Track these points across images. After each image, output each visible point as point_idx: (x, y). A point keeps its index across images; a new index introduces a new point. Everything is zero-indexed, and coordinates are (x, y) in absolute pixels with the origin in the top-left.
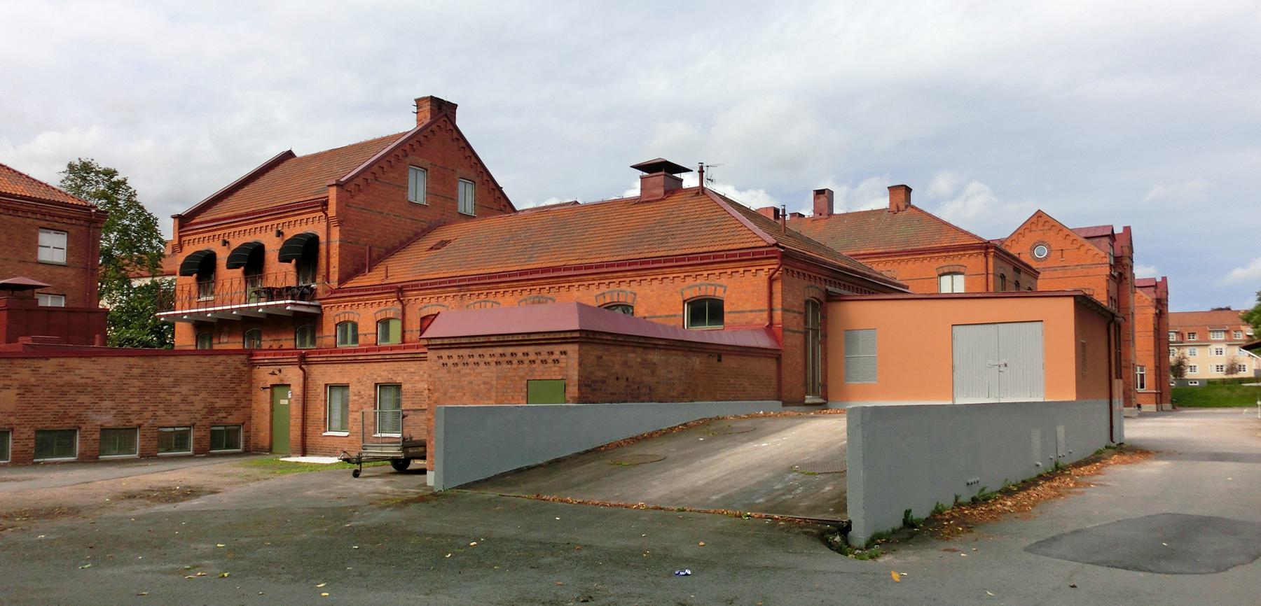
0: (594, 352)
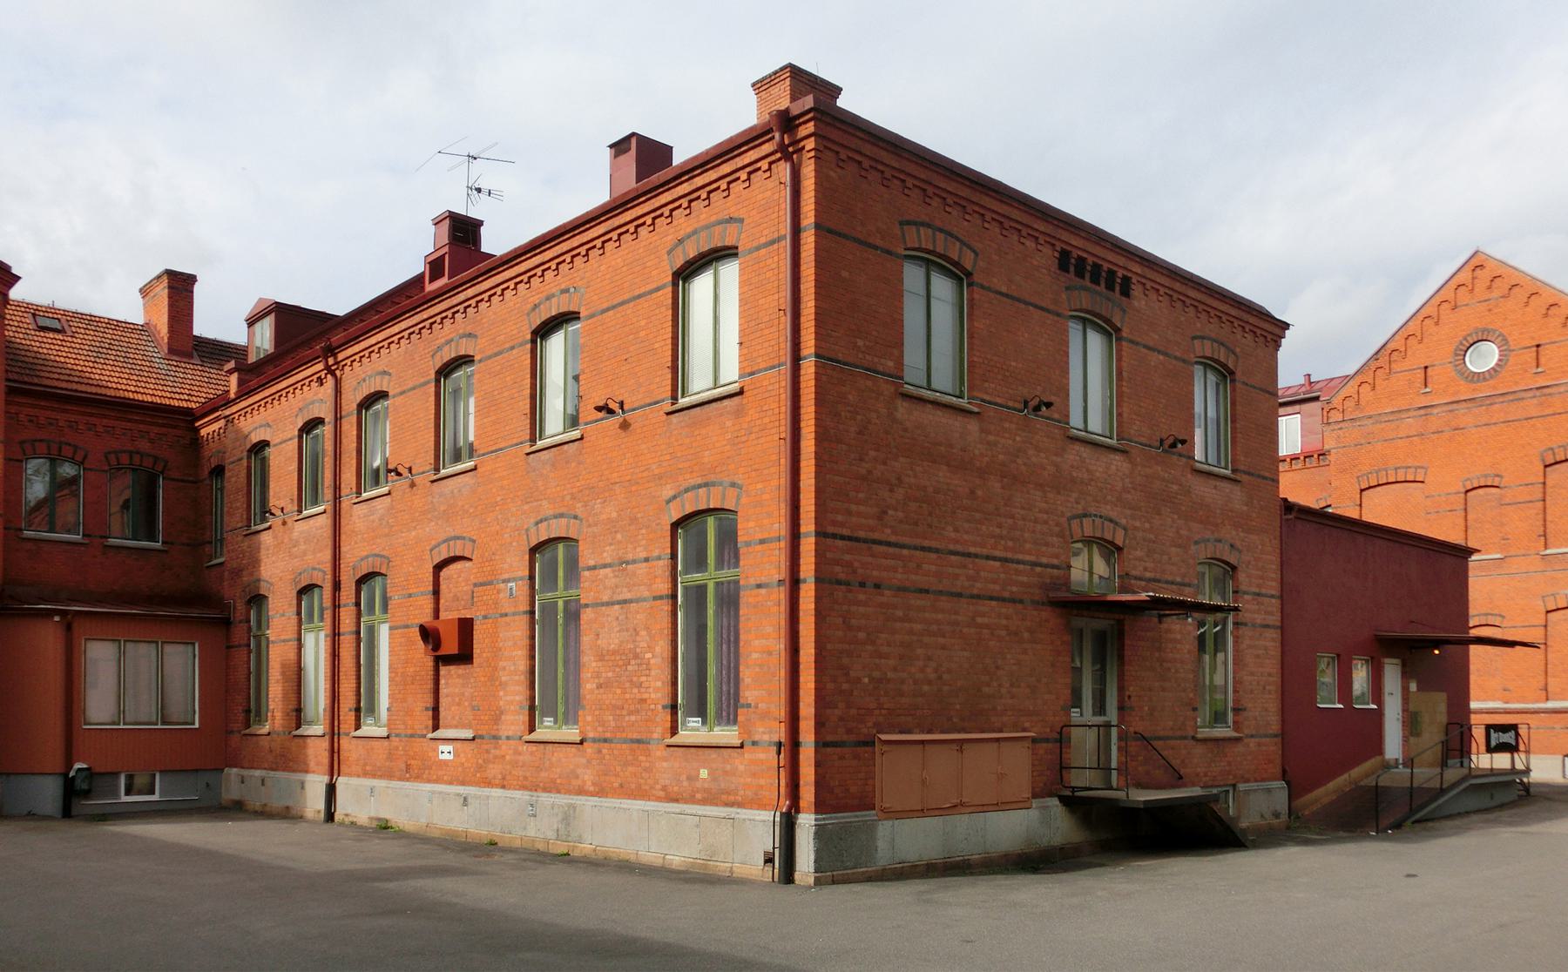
0: (1415, 765)
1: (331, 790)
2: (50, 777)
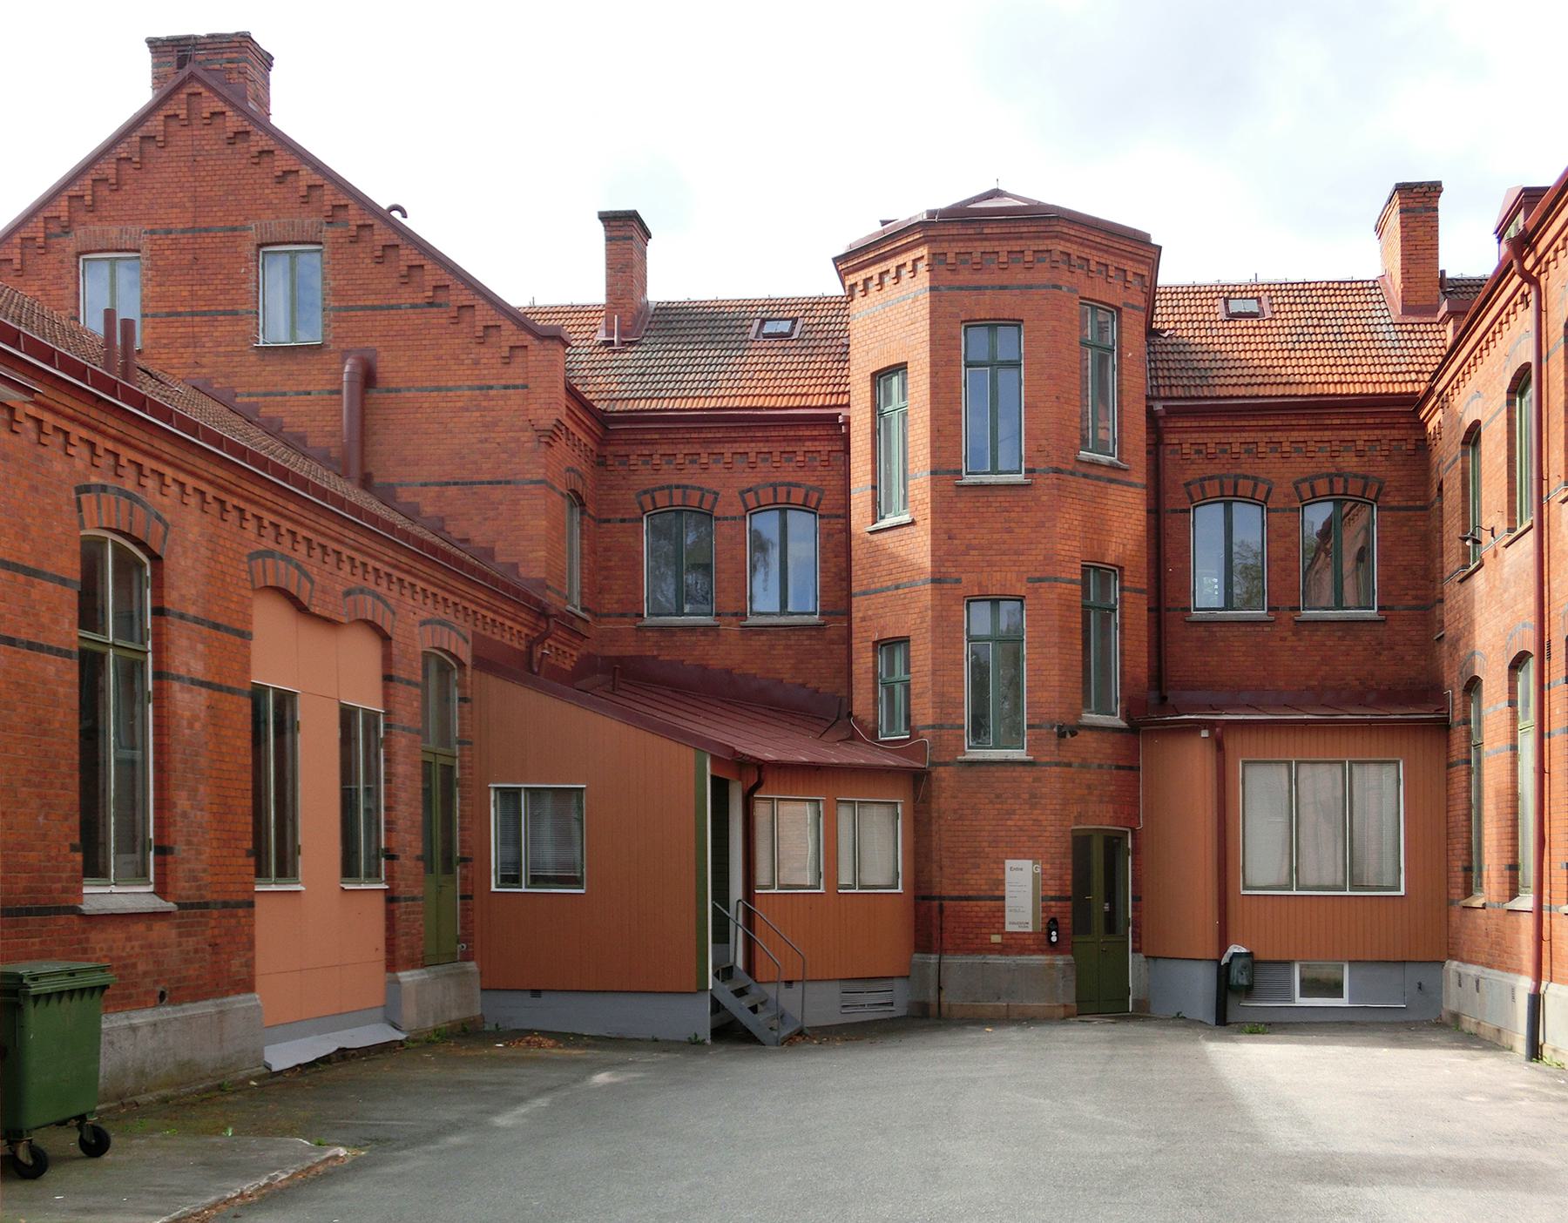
1: (1536, 1002)
2: (1202, 965)
